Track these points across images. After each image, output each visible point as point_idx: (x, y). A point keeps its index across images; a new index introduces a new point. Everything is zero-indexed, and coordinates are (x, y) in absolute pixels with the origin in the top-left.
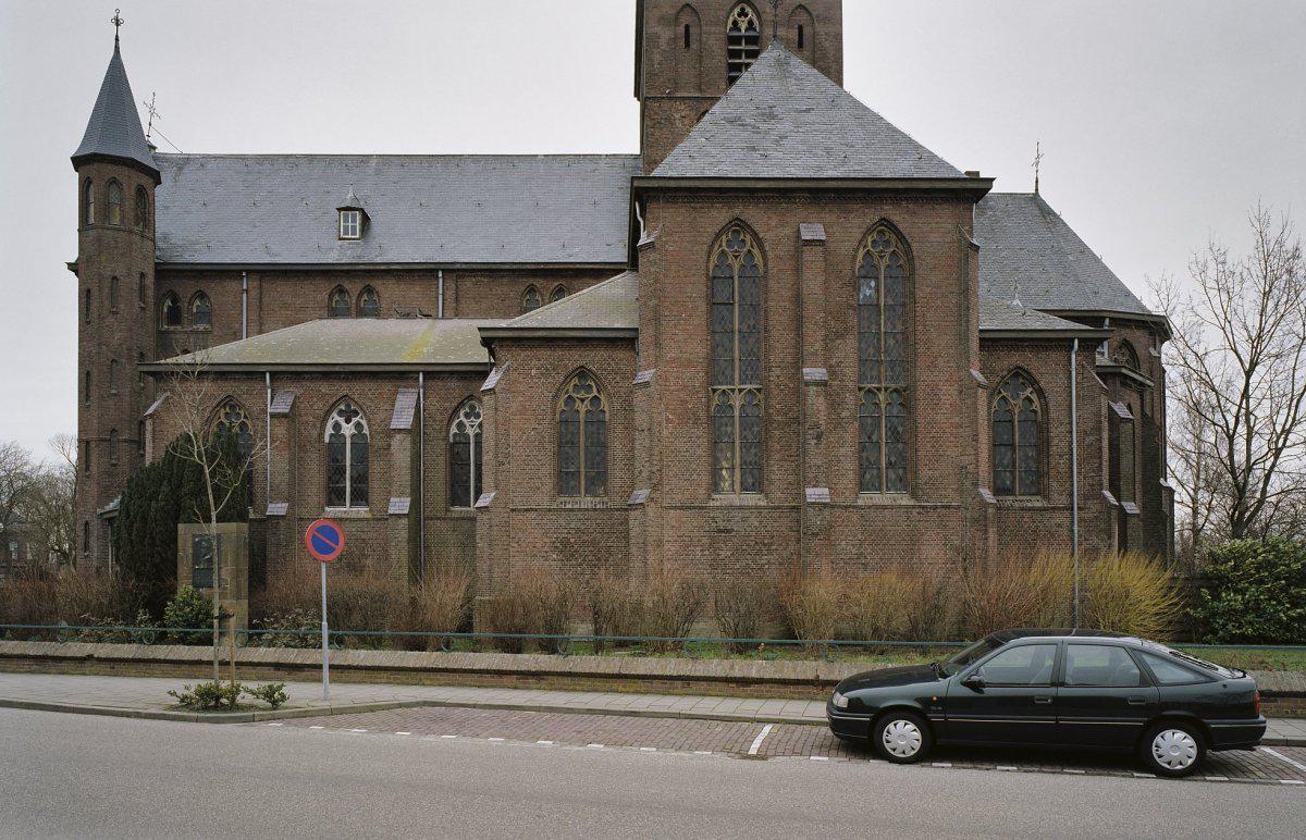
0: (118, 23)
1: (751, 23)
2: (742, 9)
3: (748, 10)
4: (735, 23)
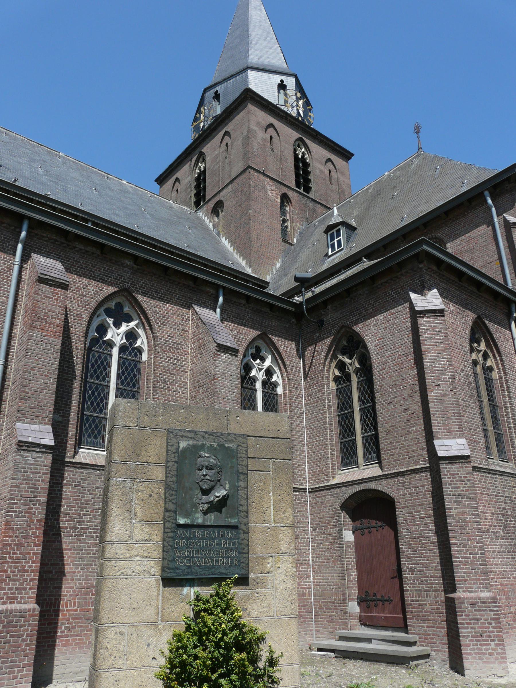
0: (417, 130)
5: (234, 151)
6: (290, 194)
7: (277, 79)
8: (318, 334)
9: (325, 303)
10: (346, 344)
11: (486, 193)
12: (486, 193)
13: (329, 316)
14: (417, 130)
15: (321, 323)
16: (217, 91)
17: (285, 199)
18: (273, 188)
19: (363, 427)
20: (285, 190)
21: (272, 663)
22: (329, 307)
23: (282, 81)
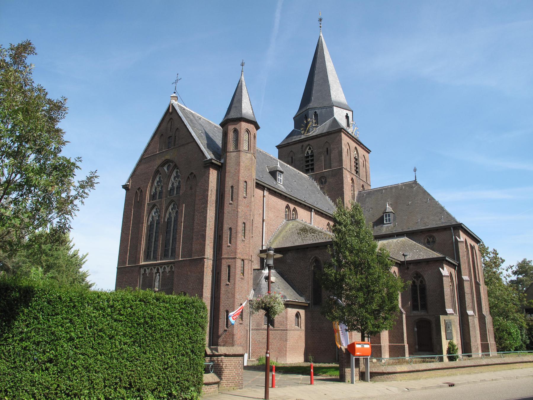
0: (415, 170)
1: (312, 151)
2: (310, 147)
3: (311, 147)
4: (308, 152)
5: (332, 155)
6: (354, 178)
7: (345, 112)
8: (406, 271)
9: (410, 264)
10: (415, 275)
11: (452, 228)
12: (452, 228)
13: (411, 267)
14: (415, 170)
15: (408, 268)
16: (316, 112)
17: (352, 179)
18: (349, 176)
19: (420, 301)
20: (352, 175)
21: (457, 349)
22: (412, 264)
23: (347, 114)
